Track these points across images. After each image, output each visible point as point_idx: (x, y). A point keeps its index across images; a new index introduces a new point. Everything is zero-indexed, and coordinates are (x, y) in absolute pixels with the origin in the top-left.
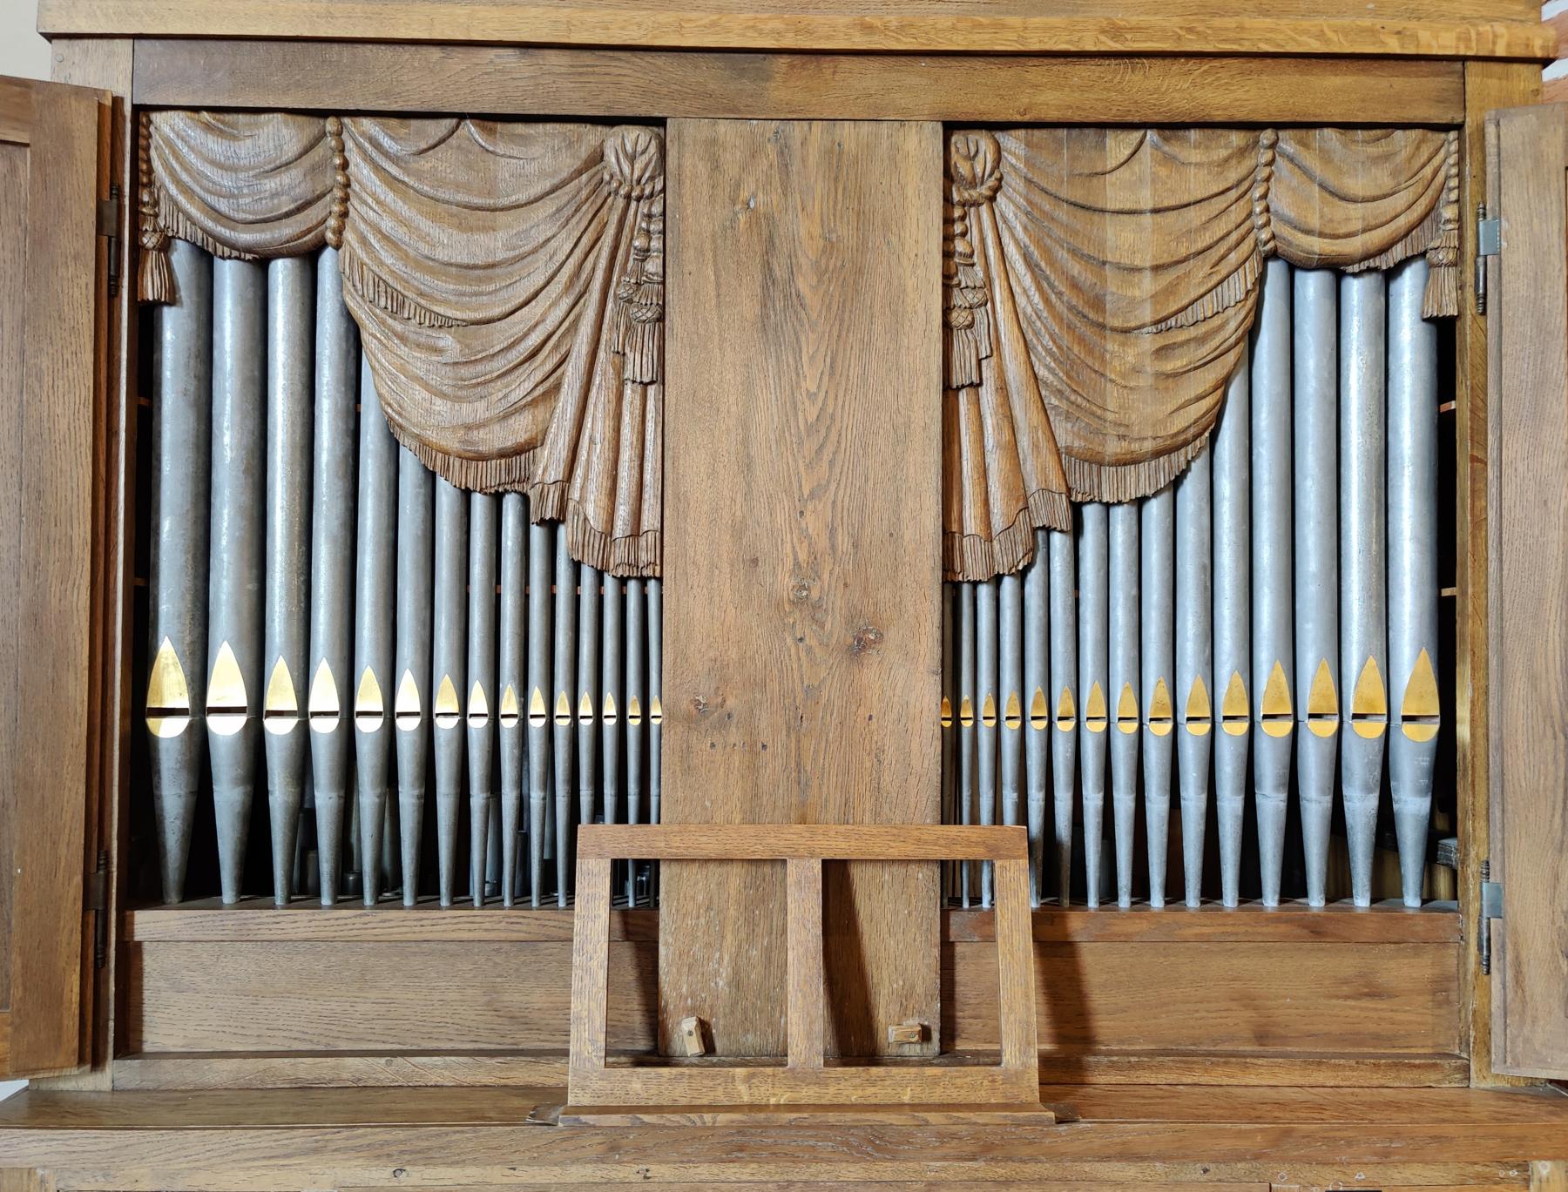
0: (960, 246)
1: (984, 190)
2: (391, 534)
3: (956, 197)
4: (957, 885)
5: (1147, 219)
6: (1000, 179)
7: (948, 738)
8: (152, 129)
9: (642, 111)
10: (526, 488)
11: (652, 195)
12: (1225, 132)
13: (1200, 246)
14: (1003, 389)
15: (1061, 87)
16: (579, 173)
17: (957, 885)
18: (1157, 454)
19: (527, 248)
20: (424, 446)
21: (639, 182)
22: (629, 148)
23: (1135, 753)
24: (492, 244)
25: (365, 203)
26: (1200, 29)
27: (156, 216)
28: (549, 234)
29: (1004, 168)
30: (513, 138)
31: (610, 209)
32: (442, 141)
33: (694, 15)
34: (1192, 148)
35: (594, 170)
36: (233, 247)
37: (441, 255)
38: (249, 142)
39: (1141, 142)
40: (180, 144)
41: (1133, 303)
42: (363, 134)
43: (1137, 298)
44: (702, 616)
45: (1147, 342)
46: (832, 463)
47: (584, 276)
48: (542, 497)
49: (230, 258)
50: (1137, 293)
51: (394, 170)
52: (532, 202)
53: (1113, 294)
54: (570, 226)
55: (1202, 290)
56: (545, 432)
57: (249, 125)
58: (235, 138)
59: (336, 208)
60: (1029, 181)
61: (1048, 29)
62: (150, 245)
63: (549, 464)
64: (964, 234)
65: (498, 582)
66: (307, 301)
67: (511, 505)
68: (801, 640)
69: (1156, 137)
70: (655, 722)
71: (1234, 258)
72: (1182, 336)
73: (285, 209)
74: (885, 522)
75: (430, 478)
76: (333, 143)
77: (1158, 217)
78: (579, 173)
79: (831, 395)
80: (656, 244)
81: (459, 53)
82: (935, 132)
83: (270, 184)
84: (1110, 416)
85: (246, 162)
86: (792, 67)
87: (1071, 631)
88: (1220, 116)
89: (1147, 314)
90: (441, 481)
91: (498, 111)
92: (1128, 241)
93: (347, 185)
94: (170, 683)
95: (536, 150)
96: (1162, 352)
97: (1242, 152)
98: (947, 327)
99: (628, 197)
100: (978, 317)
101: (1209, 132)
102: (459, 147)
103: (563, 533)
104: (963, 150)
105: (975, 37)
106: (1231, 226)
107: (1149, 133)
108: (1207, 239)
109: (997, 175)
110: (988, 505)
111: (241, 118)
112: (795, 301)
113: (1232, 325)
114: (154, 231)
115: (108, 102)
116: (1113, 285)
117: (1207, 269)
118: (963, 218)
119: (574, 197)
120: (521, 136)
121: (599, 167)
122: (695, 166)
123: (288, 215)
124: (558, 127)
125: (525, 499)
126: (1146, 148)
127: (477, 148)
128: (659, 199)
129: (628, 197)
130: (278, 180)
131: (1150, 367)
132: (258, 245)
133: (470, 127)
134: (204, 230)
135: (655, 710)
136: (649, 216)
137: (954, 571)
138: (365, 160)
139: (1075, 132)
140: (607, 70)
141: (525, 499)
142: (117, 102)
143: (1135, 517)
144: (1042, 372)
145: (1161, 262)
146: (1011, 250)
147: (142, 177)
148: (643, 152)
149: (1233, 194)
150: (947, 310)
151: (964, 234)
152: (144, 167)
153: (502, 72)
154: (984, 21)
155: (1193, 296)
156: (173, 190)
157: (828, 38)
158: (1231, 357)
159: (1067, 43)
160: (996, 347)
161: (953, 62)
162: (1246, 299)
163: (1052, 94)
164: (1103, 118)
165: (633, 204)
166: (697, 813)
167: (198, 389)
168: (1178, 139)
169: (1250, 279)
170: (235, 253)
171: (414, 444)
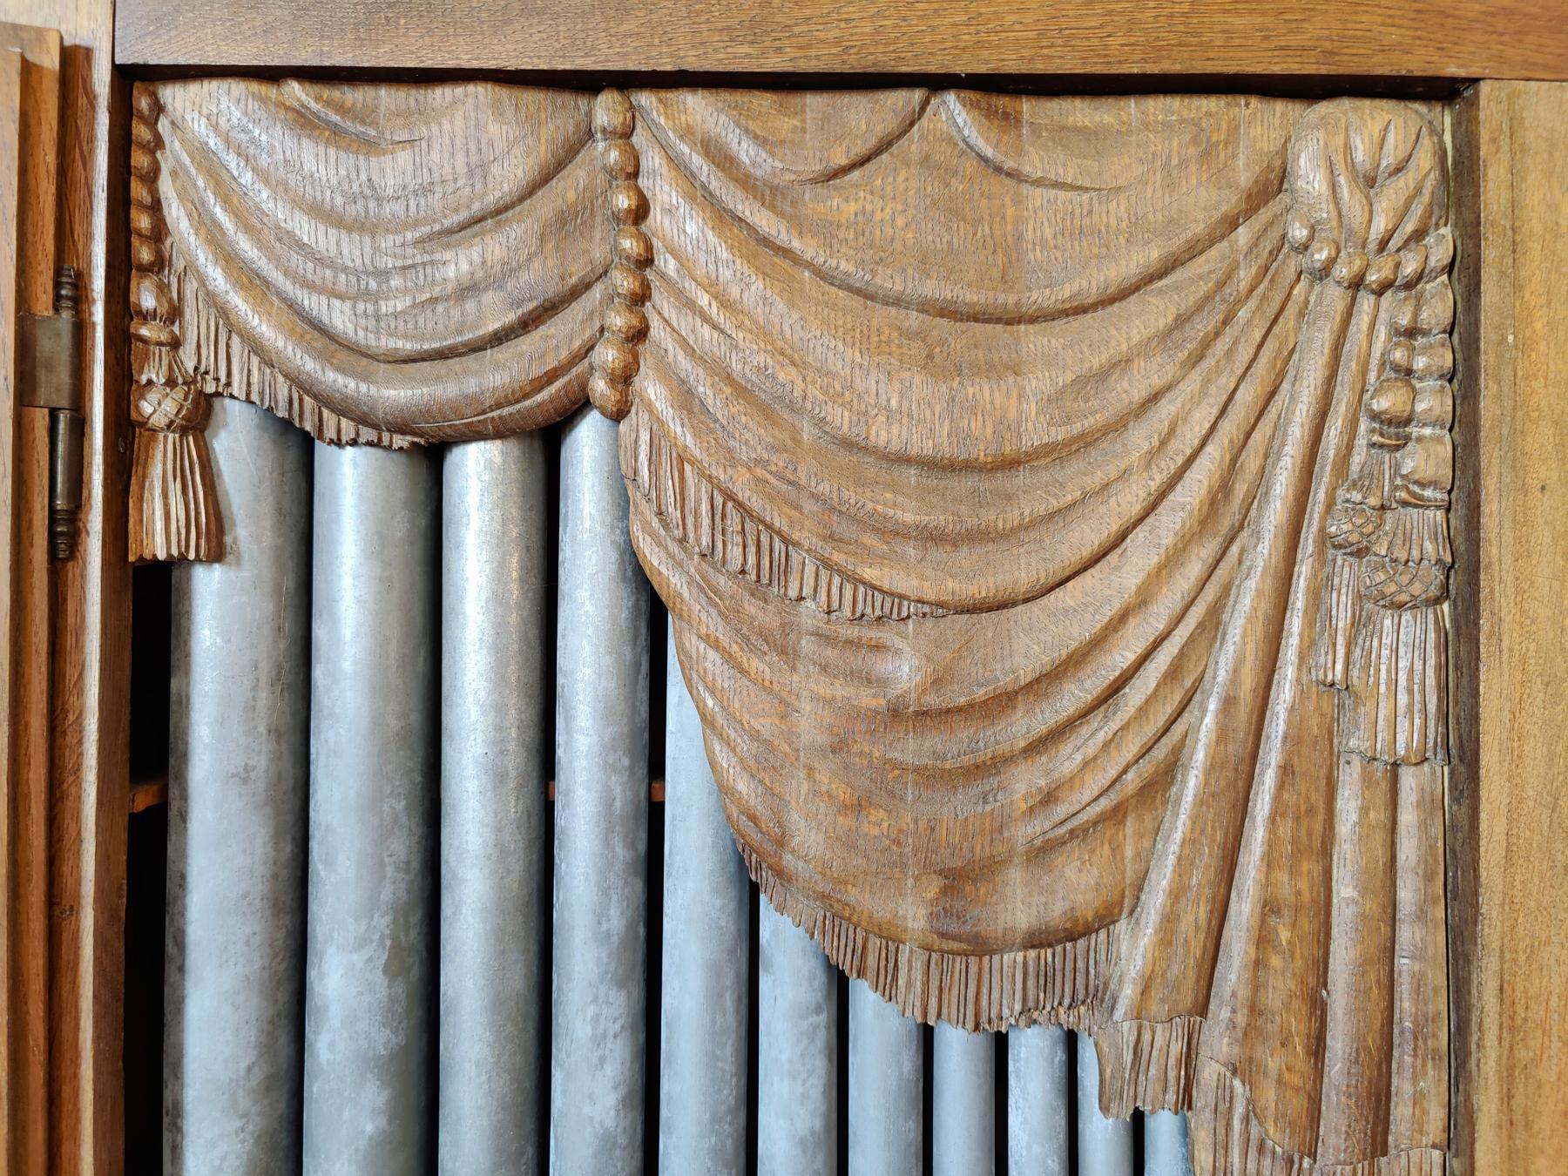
8: (163, 125)
9: (1415, 63)
19: (1099, 419)
21: (1383, 245)
22: (1361, 155)
25: (690, 305)
27: (175, 344)
28: (1157, 382)
30: (1063, 134)
35: (1264, 215)
36: (362, 420)
37: (882, 435)
38: (404, 157)
40: (232, 161)
42: (687, 133)
49: (354, 443)
51: (764, 221)
52: (1112, 300)
54: (1209, 362)
57: (407, 114)
58: (369, 146)
59: (619, 320)
62: (159, 420)
66: (536, 541)
73: (492, 326)
76: (614, 155)
80: (1433, 401)
83: (458, 264)
85: (397, 208)
91: (1040, 67)
93: (646, 261)
95: (1121, 166)
102: (925, 160)
111: (387, 97)
114: (171, 382)
115: (50, 60)
119: (1221, 285)
120: (1082, 131)
121: (1274, 207)
123: (499, 338)
127: (970, 166)
130: (475, 253)
132: (427, 413)
133: (953, 108)
134: (295, 380)
138: (690, 198)
142: (74, 59)
147: (136, 249)
148: (1399, 169)
152: (145, 254)
156: (217, 277)
167: (276, 757)
170: (367, 434)
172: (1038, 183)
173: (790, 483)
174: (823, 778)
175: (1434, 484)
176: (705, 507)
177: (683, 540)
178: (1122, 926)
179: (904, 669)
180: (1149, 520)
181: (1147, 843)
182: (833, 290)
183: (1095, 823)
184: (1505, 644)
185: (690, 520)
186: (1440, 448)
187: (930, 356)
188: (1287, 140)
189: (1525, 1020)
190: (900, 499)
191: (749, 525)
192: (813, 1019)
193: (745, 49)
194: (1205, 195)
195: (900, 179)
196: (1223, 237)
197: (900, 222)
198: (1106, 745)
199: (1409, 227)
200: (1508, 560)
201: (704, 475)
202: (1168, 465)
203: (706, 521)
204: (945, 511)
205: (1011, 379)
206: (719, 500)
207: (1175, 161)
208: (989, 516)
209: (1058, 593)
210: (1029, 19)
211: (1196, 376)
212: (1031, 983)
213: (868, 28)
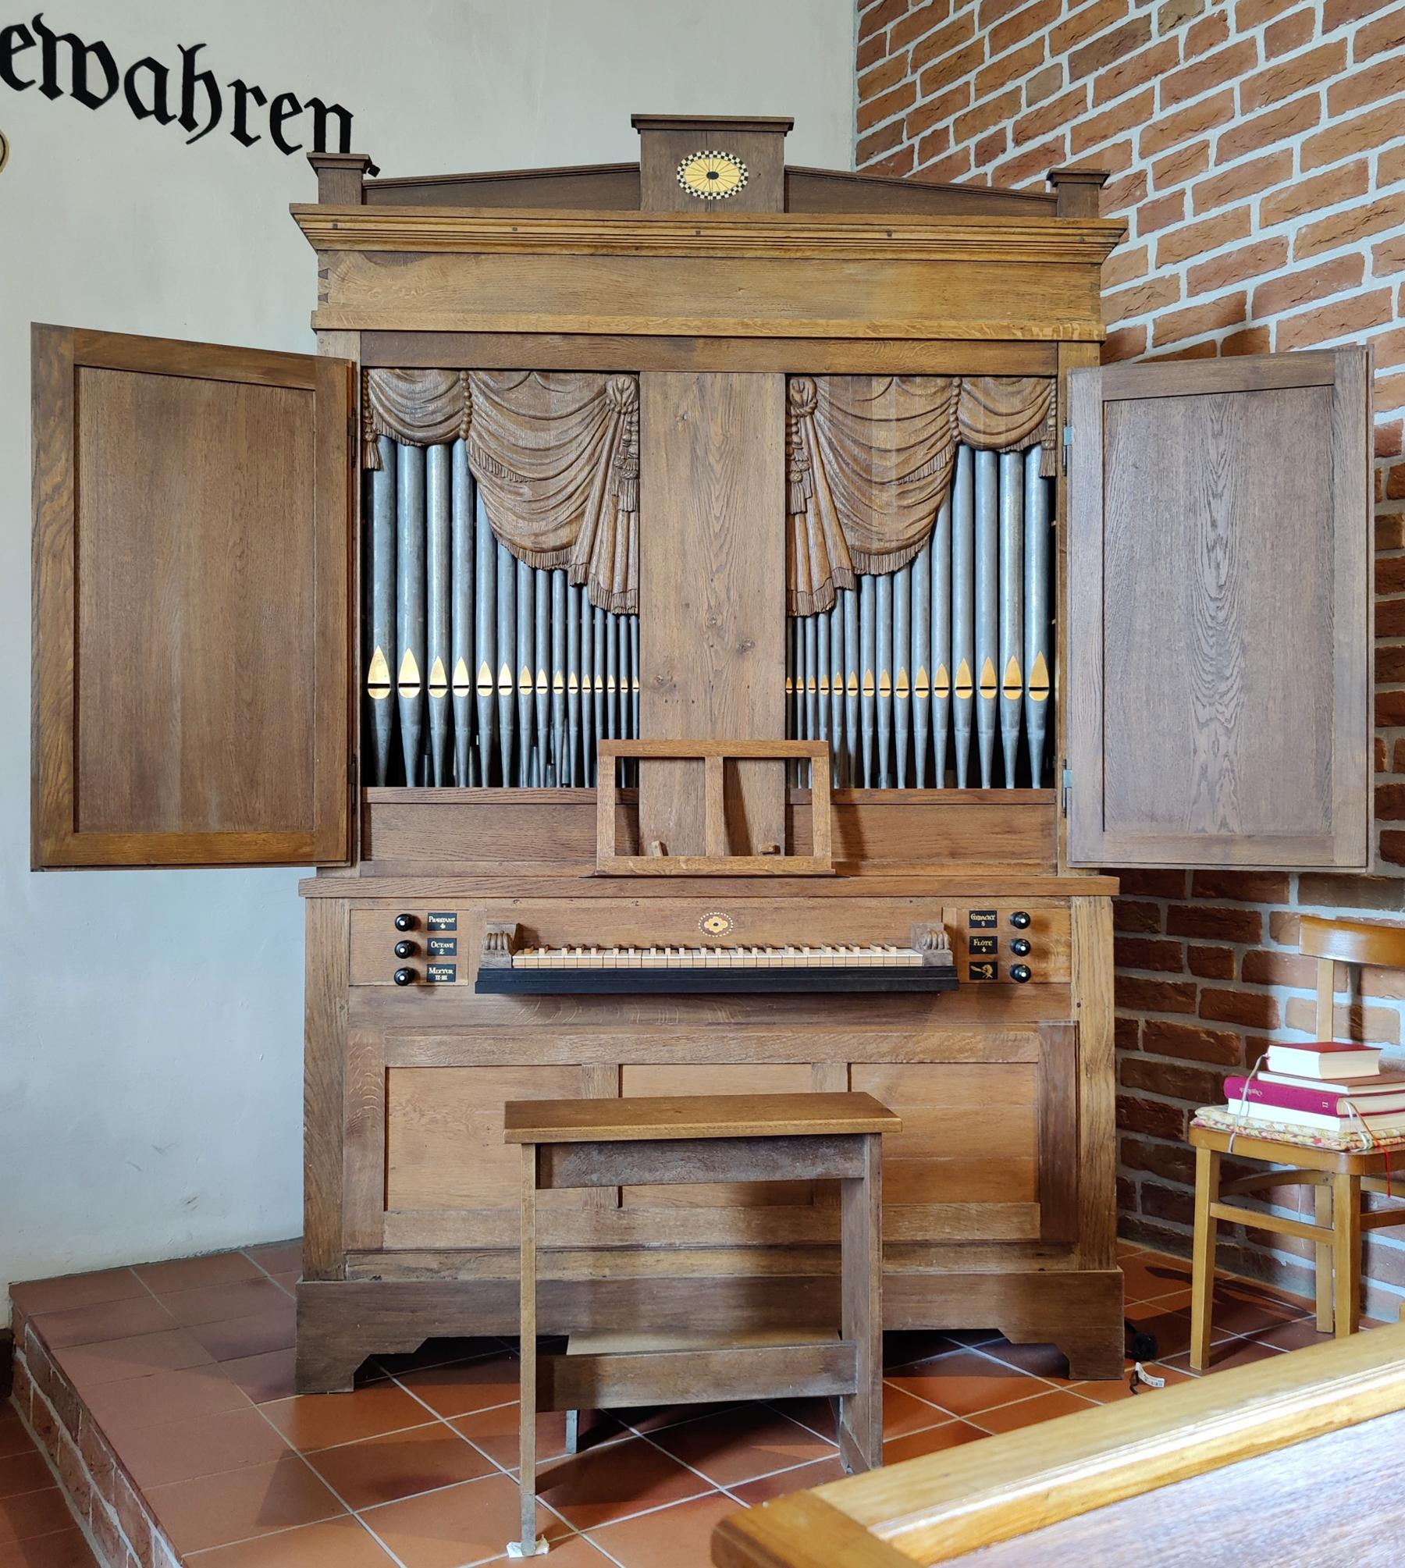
1: (807, 409)
4: (795, 768)
16: (594, 400)
17: (795, 768)
18: (899, 549)
29: (819, 397)
34: (917, 387)
43: (888, 467)
44: (662, 636)
45: (894, 490)
60: (831, 404)
63: (579, 554)
67: (558, 577)
71: (939, 445)
75: (515, 560)
78: (594, 400)
80: (635, 437)
92: (884, 437)
94: (379, 672)
96: (901, 495)
97: (943, 389)
98: (788, 481)
110: (811, 576)
126: (893, 386)
129: (619, 413)
144: (838, 505)
146: (822, 440)
150: (788, 473)
160: (814, 492)
161: (791, 342)
163: (842, 359)
166: (659, 727)
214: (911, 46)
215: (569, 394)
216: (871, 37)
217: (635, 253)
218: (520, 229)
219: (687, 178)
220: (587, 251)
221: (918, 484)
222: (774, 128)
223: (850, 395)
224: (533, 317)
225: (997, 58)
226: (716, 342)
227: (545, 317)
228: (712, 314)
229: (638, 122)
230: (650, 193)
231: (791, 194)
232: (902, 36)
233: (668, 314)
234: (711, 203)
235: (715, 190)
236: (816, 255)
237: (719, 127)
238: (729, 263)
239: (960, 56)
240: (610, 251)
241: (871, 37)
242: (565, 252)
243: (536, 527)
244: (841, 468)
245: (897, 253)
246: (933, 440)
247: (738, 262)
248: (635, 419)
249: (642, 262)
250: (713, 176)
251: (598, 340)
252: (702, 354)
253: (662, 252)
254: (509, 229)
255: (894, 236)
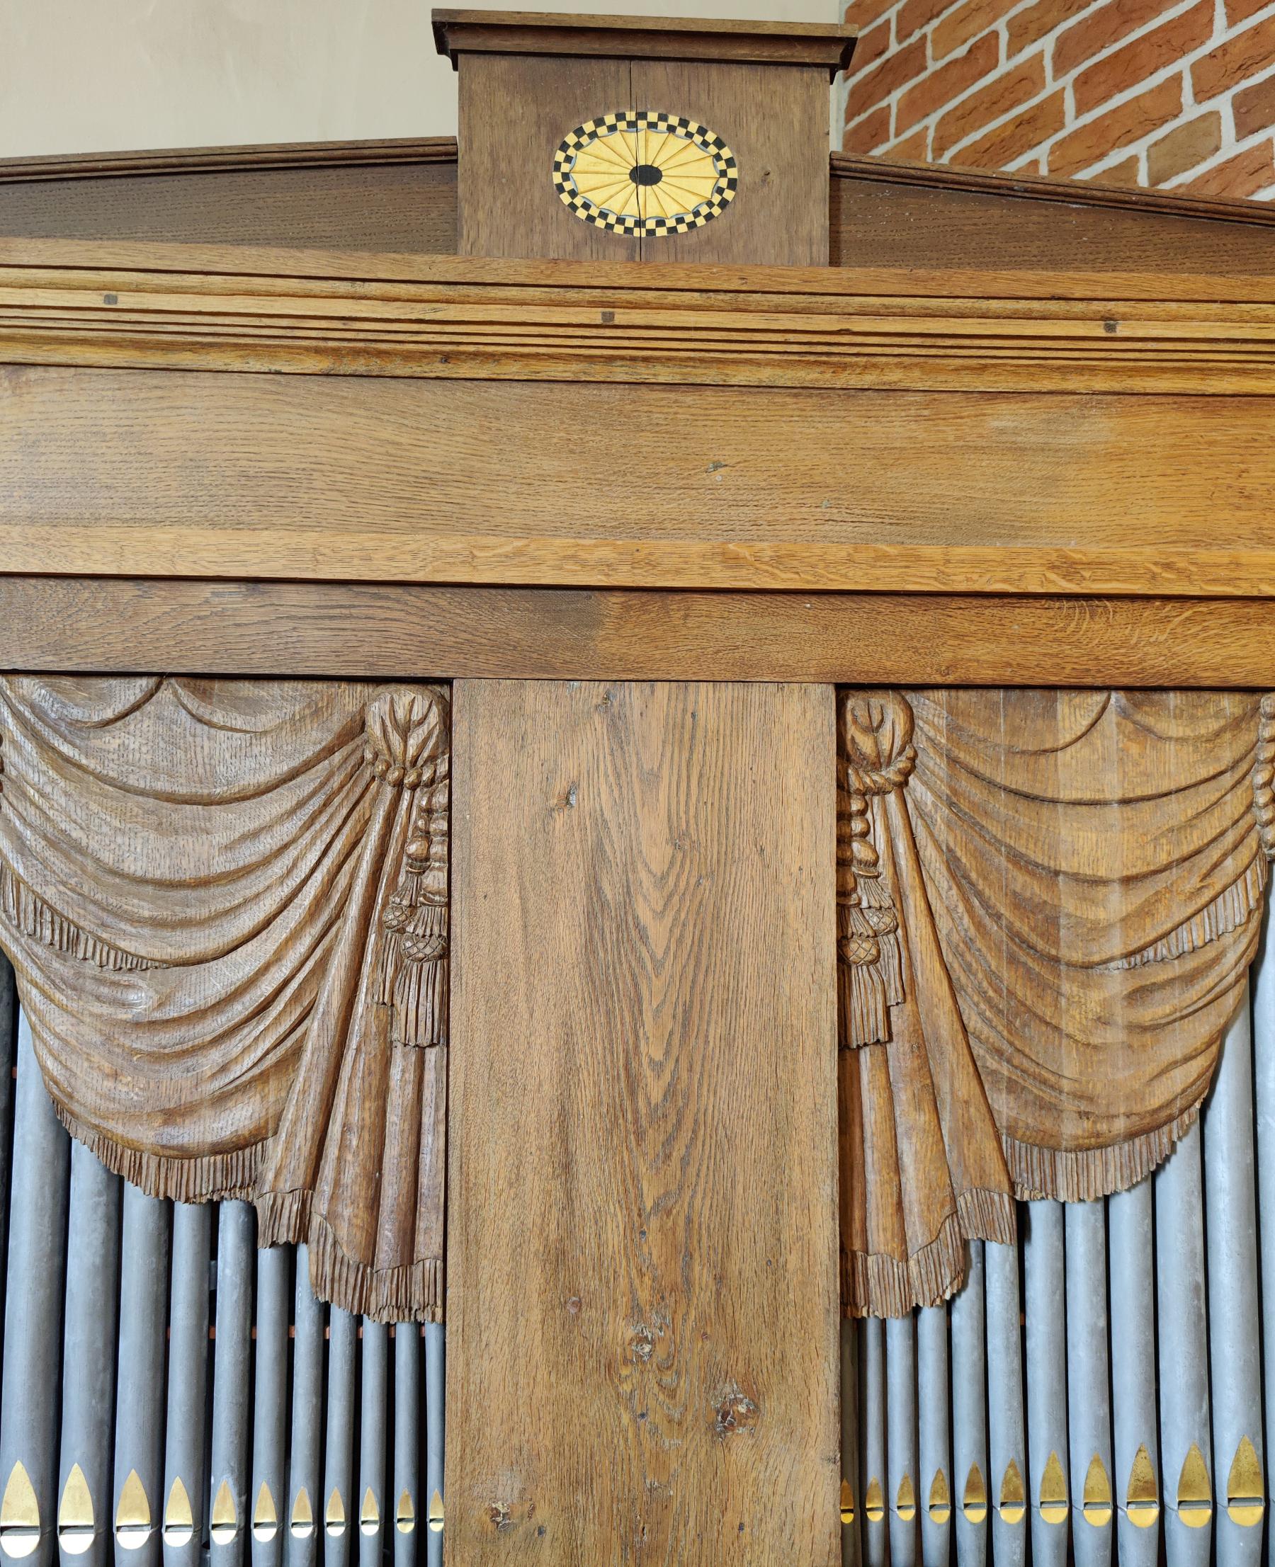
0: (859, 850)
1: (891, 774)
2: (57, 1260)
3: (854, 782)
5: (1114, 812)
6: (913, 760)
7: (850, 1541)
10: (252, 1196)
11: (432, 781)
12: (1214, 696)
13: (1187, 849)
14: (922, 1048)
15: (995, 638)
16: (330, 751)
18: (1131, 1136)
20: (106, 1144)
21: (414, 763)
22: (401, 714)
23: (1108, 1553)
24: (206, 846)
26: (1182, 564)
29: (920, 741)
31: (374, 799)
32: (136, 707)
33: (491, 540)
34: (1171, 718)
39: (1104, 709)
41: (1097, 930)
45: (1116, 983)
46: (685, 1162)
47: (336, 896)
48: (275, 1212)
50: (1101, 915)
53: (1068, 915)
54: (317, 826)
55: (1190, 911)
56: (279, 1118)
60: (953, 761)
61: (977, 562)
63: (281, 1162)
64: (864, 834)
65: (214, 1254)
67: (231, 1217)
68: (643, 1415)
69: (1124, 701)
70: (435, 1528)
71: (1230, 865)
72: (1162, 975)
74: (760, 1244)
75: (116, 1186)
77: (1128, 811)
78: (330, 751)
79: (684, 1064)
80: (438, 849)
81: (162, 590)
82: (824, 698)
84: (1066, 1085)
86: (626, 608)
87: (1017, 1402)
88: (1209, 678)
89: (1115, 944)
90: (129, 1187)
92: (1086, 845)
96: (1138, 995)
97: (1236, 724)
98: (843, 962)
99: (399, 785)
100: (885, 949)
101: (1193, 696)
103: (303, 1253)
104: (863, 720)
105: (878, 572)
106: (1227, 823)
107: (1114, 695)
108: (1195, 840)
109: (909, 752)
112: (634, 933)
113: (1231, 958)
116: (1069, 903)
117: (1195, 882)
118: (862, 813)
121: (358, 741)
122: (492, 746)
124: (299, 685)
125: (251, 1211)
126: (1111, 716)
128: (442, 786)
129: (399, 785)
131: (1121, 1014)
135: (435, 1510)
136: (429, 811)
137: (855, 1305)
139: (1015, 695)
140: (370, 612)
141: (251, 1211)
143: (1101, 1216)
144: (974, 1022)
145: (1134, 871)
146: (929, 853)
148: (421, 722)
149: (1228, 780)
150: (843, 941)
151: (864, 834)
153: (222, 615)
154: (892, 550)
155: (1178, 918)
157: (678, 572)
158: (1230, 1000)
159: (1004, 581)
160: (909, 989)
161: (848, 603)
162: (1248, 921)
163: (984, 649)
164: (1053, 680)
165: (407, 795)
168: (1152, 704)
169: (1253, 894)
171: (93, 1135)
172: (222, 728)
173: (79, 894)
174: (96, 1059)
175: (439, 893)
176: (31, 907)
177: (19, 926)
178: (270, 1141)
179: (142, 998)
180: (285, 913)
181: (283, 1094)
182: (107, 787)
183: (250, 1082)
184: (464, 979)
185: (22, 915)
186: (441, 874)
187: (160, 824)
188: (364, 705)
189: (475, 1184)
190: (142, 903)
191: (57, 919)
192: (97, 1199)
193: (51, 658)
194: (315, 735)
195: (145, 726)
196: (326, 758)
197: (144, 749)
198: (256, 1039)
199: (426, 754)
200: (465, 935)
201: (29, 888)
202: (293, 883)
203: (31, 916)
204: (167, 909)
205: (204, 836)
206: (39, 905)
207: (297, 717)
208: (191, 913)
209: (233, 954)
210: (209, 643)
211: (308, 835)
212: (219, 1174)
213: (119, 647)
214: (932, 120)
215: (251, 744)
216: (864, 116)
217: (440, 369)
218: (126, 300)
219: (580, 181)
220: (323, 364)
221: (1177, 969)
222: (806, 55)
223: (1001, 737)
224: (163, 536)
225: (1088, 118)
226: (656, 601)
227: (196, 536)
228: (643, 529)
229: (450, 33)
230: (482, 211)
231: (847, 230)
232: (915, 108)
233: (527, 530)
234: (642, 242)
235: (652, 211)
236: (915, 379)
237: (664, 49)
238: (689, 398)
239: (1020, 122)
240: (375, 366)
241: (864, 116)
242: (255, 365)
243: (175, 1082)
244: (979, 926)
245: (1121, 373)
246: (1215, 853)
247: (710, 396)
248: (441, 799)
249: (461, 394)
250: (646, 175)
251: (339, 595)
252: (614, 637)
253: (512, 369)
254: (95, 300)
255: (1122, 330)
